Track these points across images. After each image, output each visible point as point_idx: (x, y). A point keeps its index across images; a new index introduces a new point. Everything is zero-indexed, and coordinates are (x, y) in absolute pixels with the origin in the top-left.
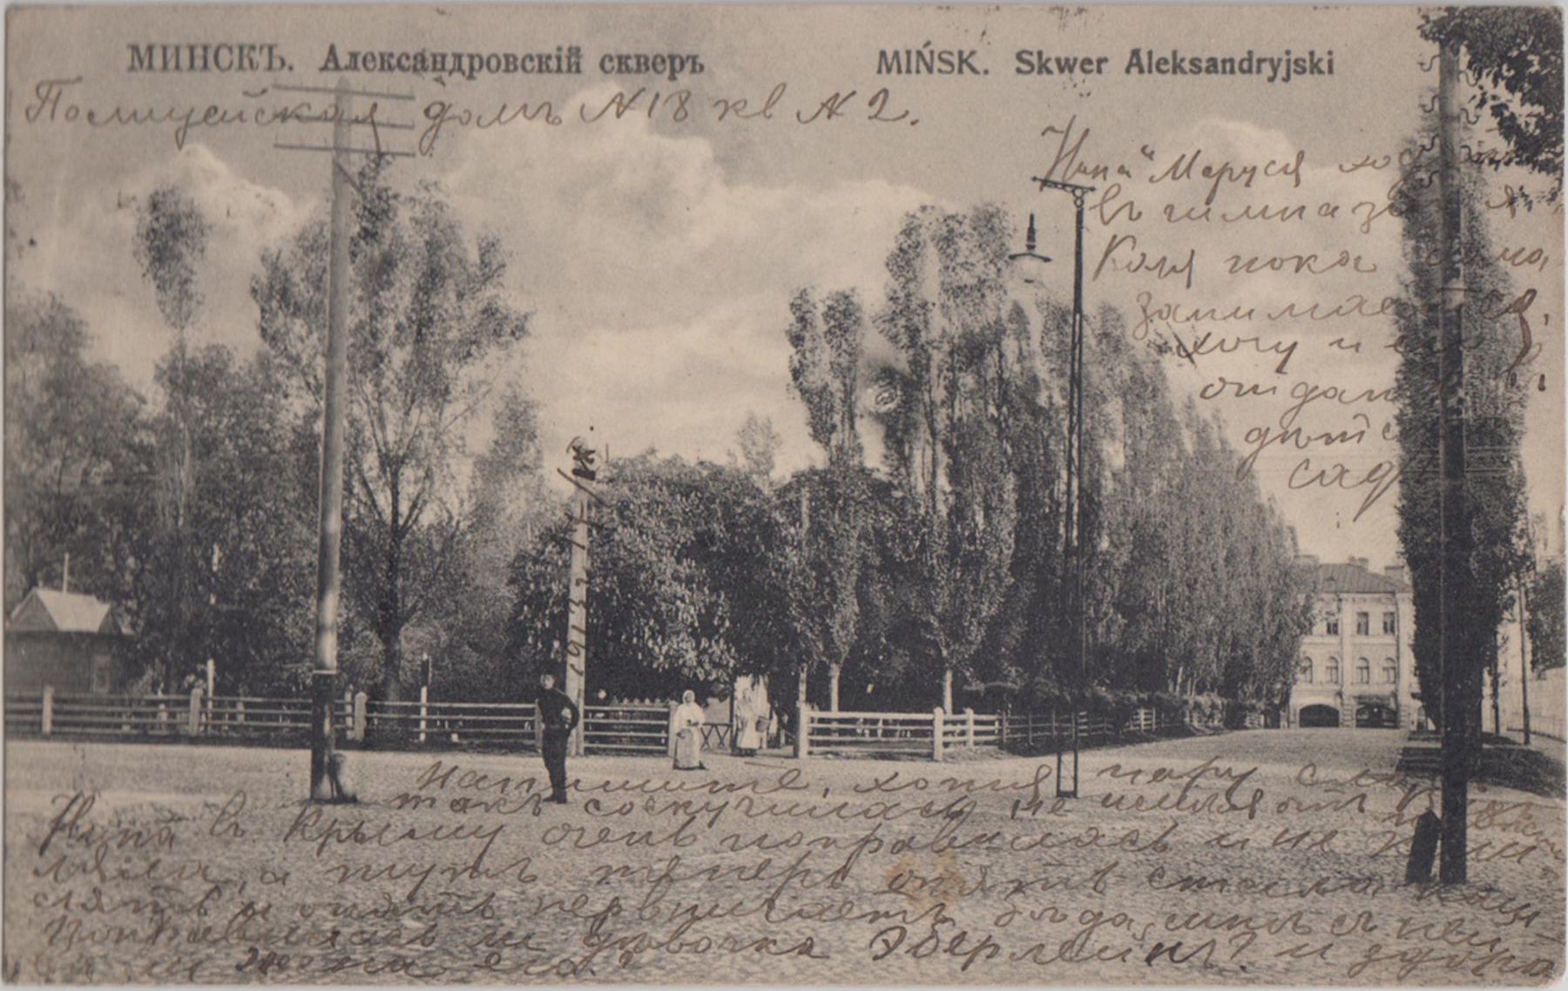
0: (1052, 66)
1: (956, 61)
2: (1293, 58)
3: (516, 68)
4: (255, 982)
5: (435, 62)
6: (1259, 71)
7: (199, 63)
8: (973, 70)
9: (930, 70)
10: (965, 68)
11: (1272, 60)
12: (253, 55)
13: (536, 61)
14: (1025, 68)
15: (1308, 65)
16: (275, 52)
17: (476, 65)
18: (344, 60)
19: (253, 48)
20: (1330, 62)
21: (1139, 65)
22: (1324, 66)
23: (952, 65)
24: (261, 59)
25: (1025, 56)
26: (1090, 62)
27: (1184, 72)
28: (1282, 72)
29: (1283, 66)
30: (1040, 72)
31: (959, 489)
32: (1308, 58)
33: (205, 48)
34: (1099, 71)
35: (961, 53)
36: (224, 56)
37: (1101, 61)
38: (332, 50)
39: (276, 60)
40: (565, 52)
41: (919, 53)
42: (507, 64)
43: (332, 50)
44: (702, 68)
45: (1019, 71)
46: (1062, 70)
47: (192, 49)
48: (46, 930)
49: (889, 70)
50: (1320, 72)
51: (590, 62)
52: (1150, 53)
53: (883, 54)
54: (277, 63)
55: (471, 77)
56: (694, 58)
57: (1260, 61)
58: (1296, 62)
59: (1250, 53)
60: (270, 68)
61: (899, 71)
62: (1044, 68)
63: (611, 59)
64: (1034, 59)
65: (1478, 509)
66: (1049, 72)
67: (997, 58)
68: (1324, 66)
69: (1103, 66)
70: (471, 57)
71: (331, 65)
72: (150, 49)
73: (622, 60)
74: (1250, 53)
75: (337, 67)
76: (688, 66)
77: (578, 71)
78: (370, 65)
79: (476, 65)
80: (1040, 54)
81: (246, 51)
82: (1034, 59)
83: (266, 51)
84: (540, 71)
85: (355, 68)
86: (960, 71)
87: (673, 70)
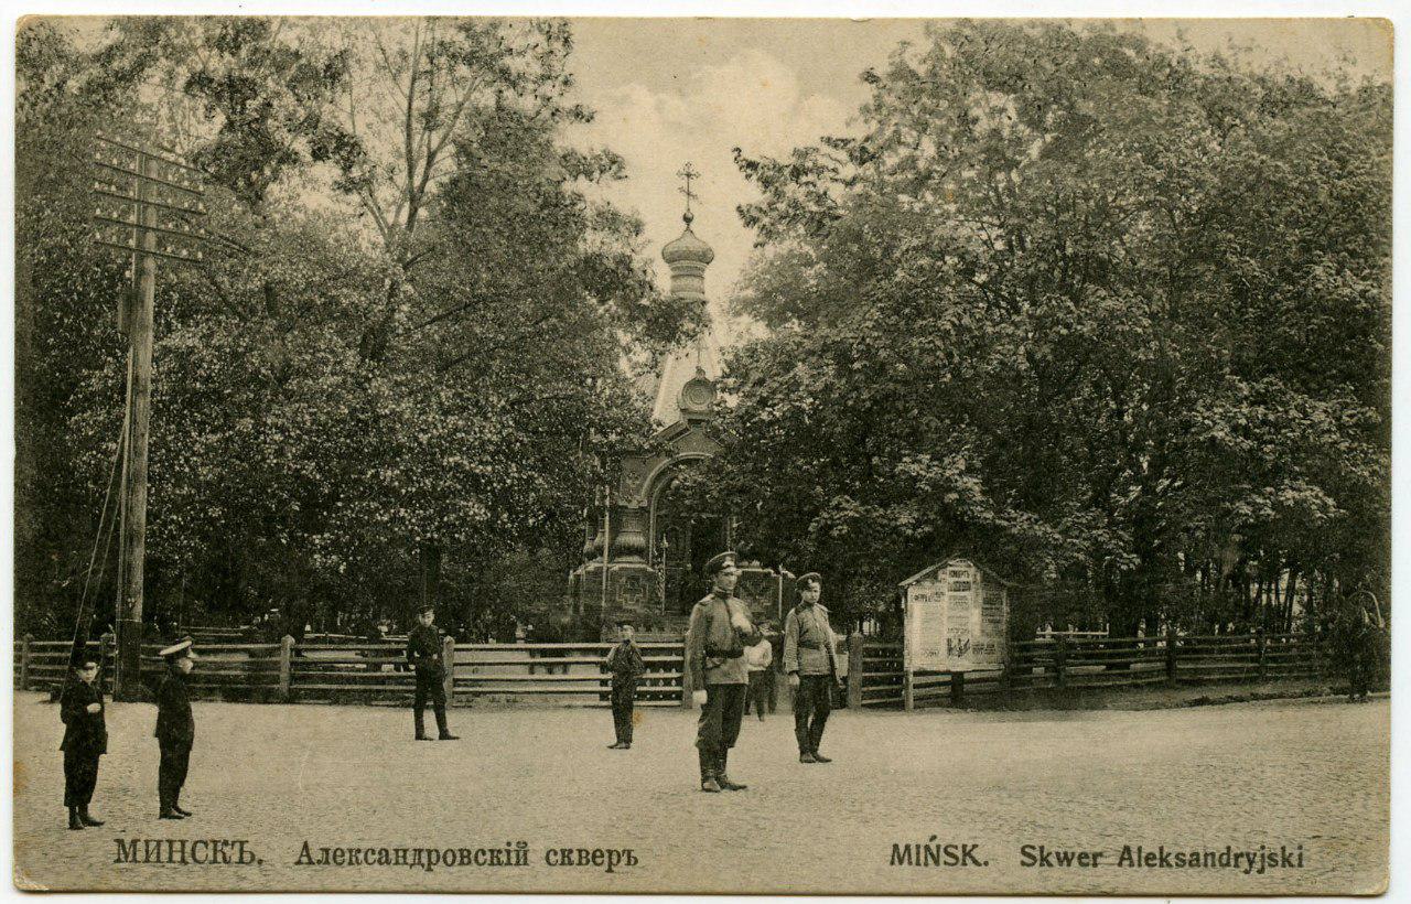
0: (1053, 859)
2: (1267, 852)
3: (588, 862)
6: (1236, 866)
7: (177, 857)
8: (976, 862)
9: (937, 862)
10: (968, 861)
11: (1248, 855)
13: (488, 856)
15: (1279, 859)
17: (434, 859)
18: (317, 855)
19: (226, 843)
20: (1300, 855)
21: (1130, 858)
22: (1294, 861)
23: (956, 858)
25: (950, 850)
26: (1087, 856)
27: (1169, 865)
28: (1257, 866)
29: (1258, 859)
30: (1041, 865)
31: (622, 554)
32: (1279, 852)
33: (183, 843)
35: (964, 846)
36: (201, 853)
37: (1095, 856)
38: (306, 846)
40: (513, 847)
41: (927, 848)
42: (462, 857)
43: (306, 846)
44: (636, 861)
45: (1023, 863)
46: (1060, 862)
48: (132, 870)
49: (901, 862)
50: (1291, 865)
52: (1140, 849)
53: (896, 847)
55: (429, 870)
56: (629, 852)
57: (1237, 856)
58: (1270, 857)
59: (1229, 848)
62: (1045, 860)
63: (484, 853)
64: (1036, 853)
66: (1050, 865)
67: (1001, 851)
68: (1294, 861)
69: (1099, 860)
70: (429, 852)
71: (305, 859)
72: (134, 842)
73: (566, 853)
74: (1229, 848)
75: (311, 862)
76: (624, 859)
77: (525, 864)
78: (339, 860)
79: (434, 859)
80: (1042, 848)
81: (219, 847)
82: (1036, 853)
83: (237, 846)
84: (492, 864)
85: (327, 862)
86: (965, 864)
87: (610, 863)
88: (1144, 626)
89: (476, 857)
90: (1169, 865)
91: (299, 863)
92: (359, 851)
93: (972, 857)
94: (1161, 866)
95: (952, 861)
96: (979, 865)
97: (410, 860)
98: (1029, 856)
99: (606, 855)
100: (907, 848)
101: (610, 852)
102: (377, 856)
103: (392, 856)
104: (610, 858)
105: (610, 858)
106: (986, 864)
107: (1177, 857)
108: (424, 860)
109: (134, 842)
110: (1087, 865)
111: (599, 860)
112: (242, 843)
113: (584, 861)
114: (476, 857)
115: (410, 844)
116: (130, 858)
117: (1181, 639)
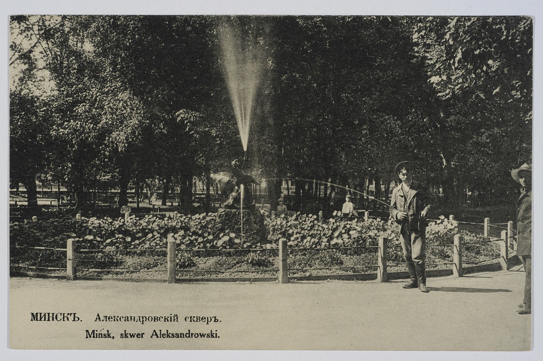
0: (128, 335)
4: (9, 184)
7: (51, 319)
22: (214, 335)
27: (170, 337)
33: (53, 314)
34: (142, 337)
38: (98, 315)
40: (172, 316)
43: (98, 315)
51: (181, 318)
60: (74, 320)
66: (127, 337)
68: (214, 335)
70: (143, 317)
72: (37, 314)
83: (73, 315)
92: (194, 317)
102: (124, 319)
106: (113, 338)
108: (141, 320)
109: (37, 314)
111: (111, 320)
112: (75, 314)
117: (303, 151)
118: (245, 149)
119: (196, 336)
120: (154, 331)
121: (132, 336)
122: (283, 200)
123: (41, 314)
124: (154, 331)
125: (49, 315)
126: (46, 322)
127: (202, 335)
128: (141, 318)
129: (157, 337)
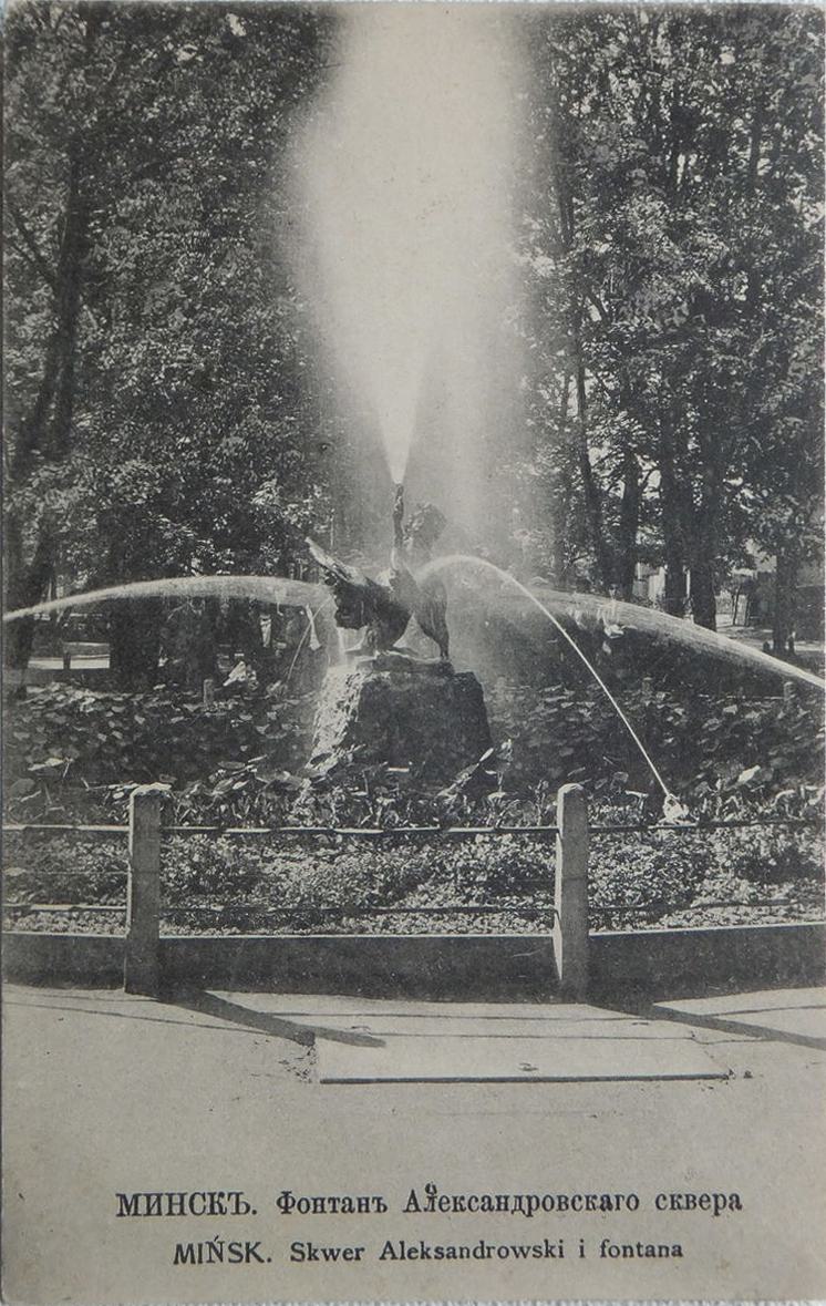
0: (320, 1254)
1: (244, 1252)
5: (499, 1203)
7: (176, 1209)
8: (261, 1260)
12: (222, 1201)
14: (299, 1256)
16: (382, 1202)
19: (221, 1195)
20: (561, 1248)
21: (392, 1251)
22: (556, 1252)
24: (229, 1205)
27: (553, 1256)
34: (358, 1258)
35: (248, 1245)
36: (199, 1204)
39: (242, 1207)
41: (211, 1245)
47: (170, 1196)
53: (179, 1248)
54: (243, 1208)
59: (482, 1242)
61: (193, 1262)
65: (516, 172)
66: (317, 1259)
68: (556, 1252)
70: (529, 1198)
71: (413, 1208)
72: (136, 1197)
75: (417, 1209)
80: (310, 1245)
81: (216, 1198)
83: (684, 1198)
86: (248, 1261)
87: (717, 1207)
88: (145, 166)
89: (573, 1202)
90: (429, 1257)
91: (408, 1210)
93: (256, 1256)
94: (422, 1257)
95: (237, 1258)
96: (262, 1261)
97: (511, 1207)
98: (238, 1253)
99: (712, 1199)
100: (190, 1247)
101: (716, 1197)
102: (480, 1204)
103: (494, 1203)
104: (716, 1202)
105: (716, 1202)
106: (269, 1260)
107: (436, 1250)
108: (525, 1206)
109: (136, 1197)
110: (351, 1259)
112: (238, 1195)
113: (691, 1205)
114: (573, 1202)
115: (512, 1192)
116: (132, 1211)
118: (226, 684)
119: (503, 1252)
120: (389, 1244)
121: (331, 1255)
122: (263, 629)
123: (170, 1196)
124: (389, 1244)
125: (315, 1203)
126: (164, 1218)
127: (521, 1252)
128: (525, 1201)
129: (394, 1257)
